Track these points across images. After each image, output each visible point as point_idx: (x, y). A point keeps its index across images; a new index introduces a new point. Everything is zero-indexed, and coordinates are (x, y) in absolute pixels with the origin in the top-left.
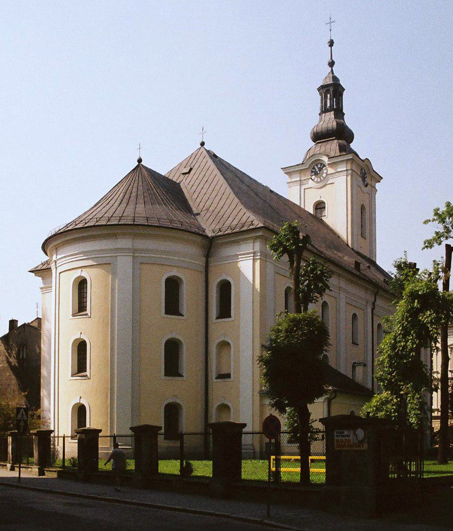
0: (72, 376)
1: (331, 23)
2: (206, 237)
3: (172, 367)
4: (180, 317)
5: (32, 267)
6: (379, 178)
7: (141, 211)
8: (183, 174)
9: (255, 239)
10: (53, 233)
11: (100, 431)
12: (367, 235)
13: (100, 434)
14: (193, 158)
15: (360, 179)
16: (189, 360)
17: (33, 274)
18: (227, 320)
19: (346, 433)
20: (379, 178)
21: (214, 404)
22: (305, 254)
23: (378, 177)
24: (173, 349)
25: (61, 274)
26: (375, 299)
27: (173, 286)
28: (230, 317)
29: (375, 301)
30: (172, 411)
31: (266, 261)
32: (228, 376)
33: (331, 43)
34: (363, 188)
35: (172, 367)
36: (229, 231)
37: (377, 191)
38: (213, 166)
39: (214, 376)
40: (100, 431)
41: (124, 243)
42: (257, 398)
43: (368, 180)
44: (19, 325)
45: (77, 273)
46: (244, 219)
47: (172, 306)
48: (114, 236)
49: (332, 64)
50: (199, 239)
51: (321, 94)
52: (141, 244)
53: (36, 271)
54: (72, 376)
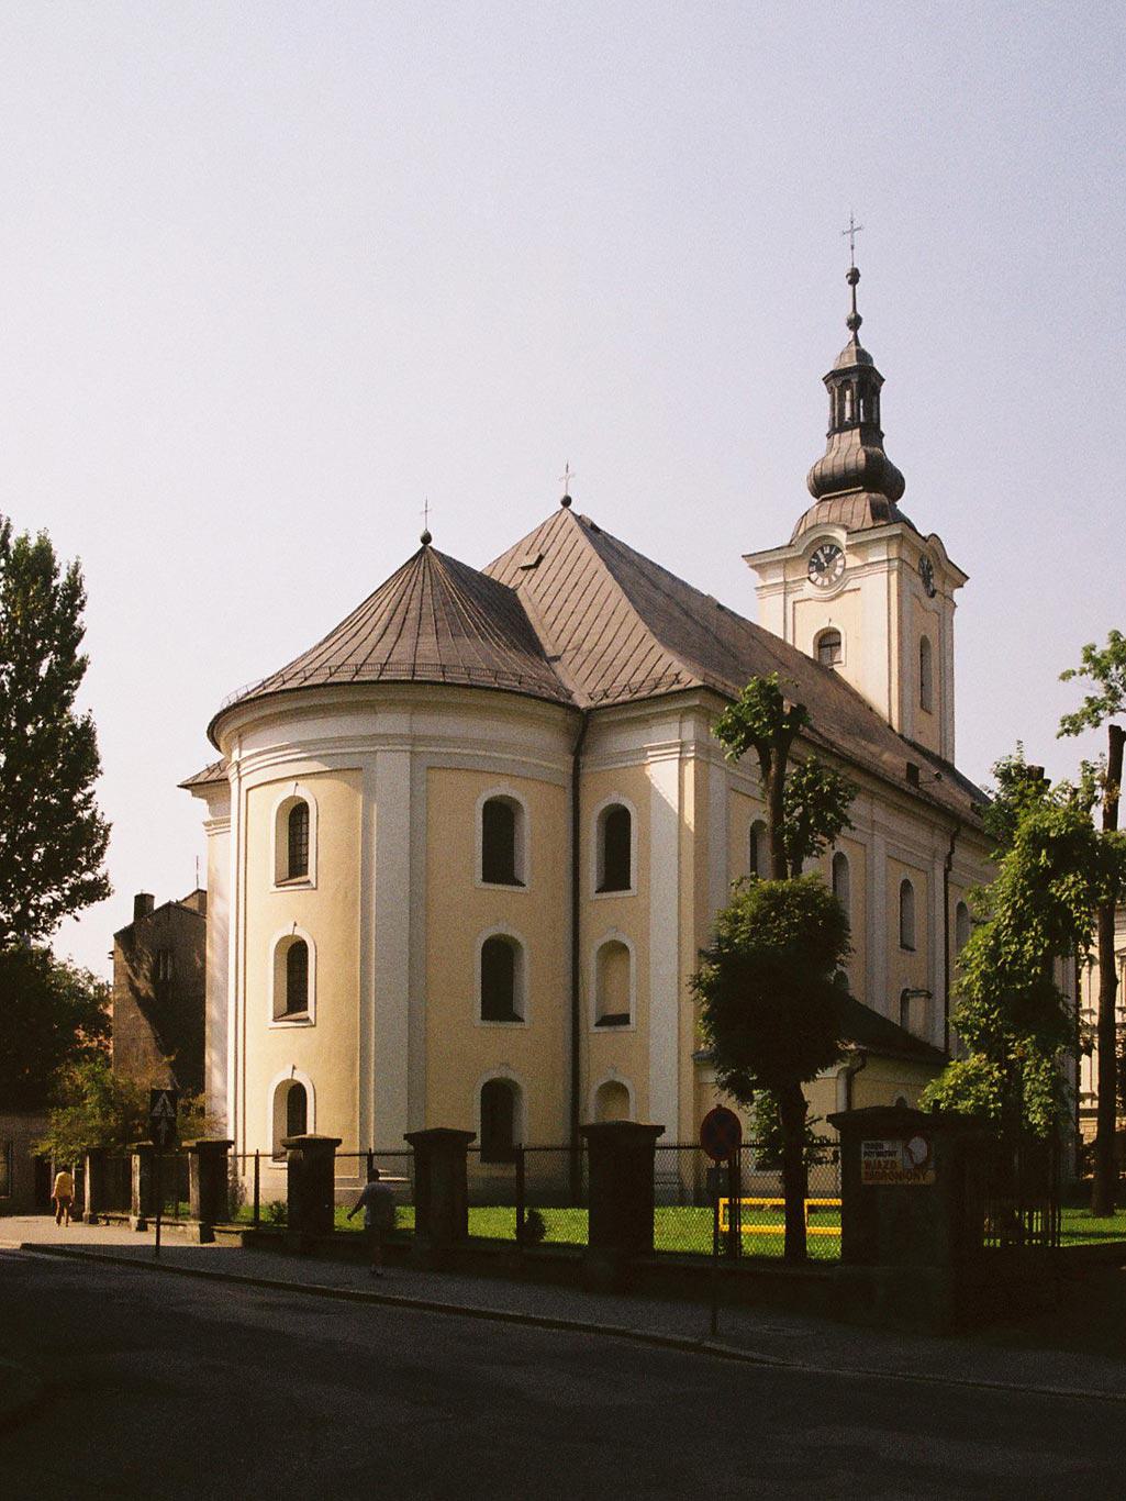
0: (276, 1019)
1: (852, 231)
2: (575, 709)
3: (499, 1000)
4: (515, 888)
5: (186, 777)
6: (960, 579)
7: (429, 651)
8: (523, 568)
9: (684, 713)
10: (234, 700)
11: (339, 1142)
12: (934, 704)
13: (338, 1150)
14: (545, 532)
15: (919, 580)
16: (537, 983)
17: (189, 792)
18: (479, 870)
19: (887, 1147)
20: (960, 579)
21: (593, 1083)
22: (796, 747)
23: (957, 576)
24: (500, 959)
25: (250, 792)
26: (952, 844)
27: (500, 819)
28: (628, 887)
29: (952, 852)
30: (499, 1098)
31: (708, 763)
32: (624, 1019)
33: (854, 277)
34: (925, 599)
35: (499, 1000)
36: (626, 697)
37: (955, 606)
38: (590, 551)
39: (593, 1020)
40: (339, 1142)
41: (392, 722)
42: (689, 1068)
43: (936, 582)
44: (157, 905)
45: (287, 791)
46: (660, 669)
47: (499, 864)
48: (369, 707)
50: (557, 714)
51: (831, 391)
52: (429, 724)
53: (194, 786)
54: (276, 1019)
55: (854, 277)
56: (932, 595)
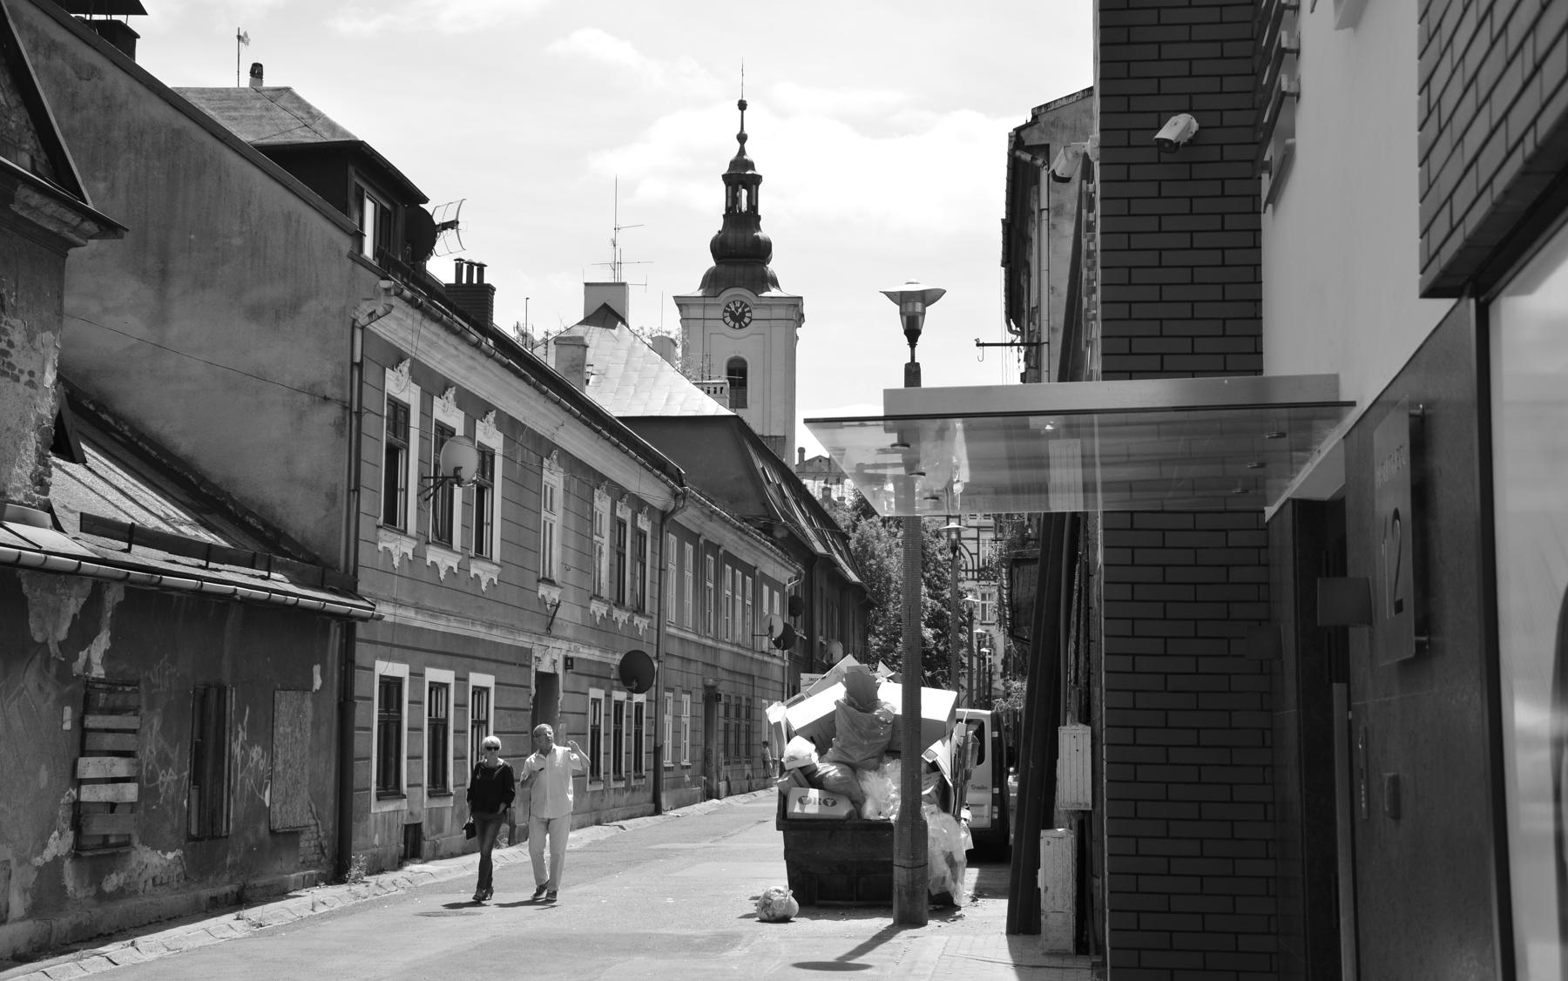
33: (742, 105)
49: (742, 138)
55: (742, 105)
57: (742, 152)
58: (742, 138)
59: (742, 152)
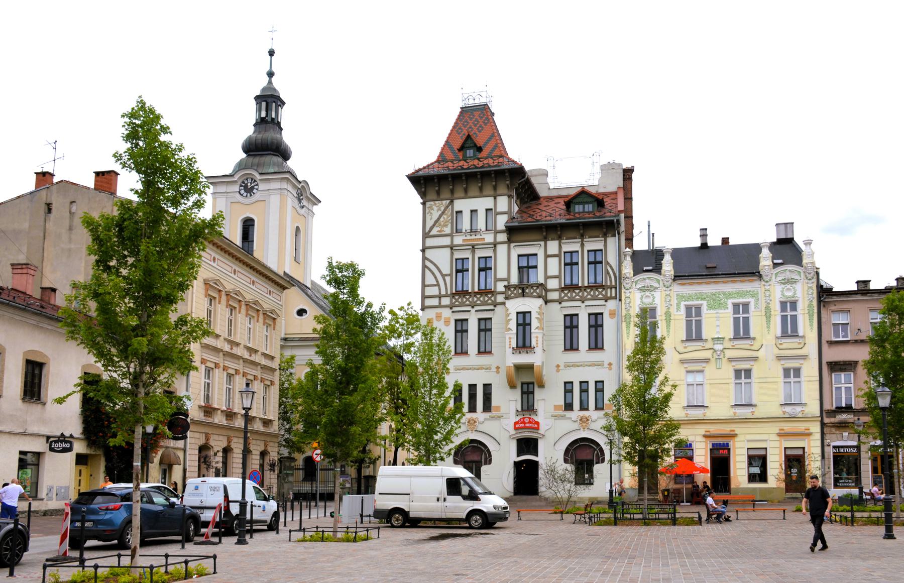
15: (296, 201)
33: (271, 53)
43: (304, 202)
44: (56, 180)
49: (271, 74)
55: (271, 53)
56: (303, 207)
57: (270, 82)
58: (271, 74)
59: (270, 82)
